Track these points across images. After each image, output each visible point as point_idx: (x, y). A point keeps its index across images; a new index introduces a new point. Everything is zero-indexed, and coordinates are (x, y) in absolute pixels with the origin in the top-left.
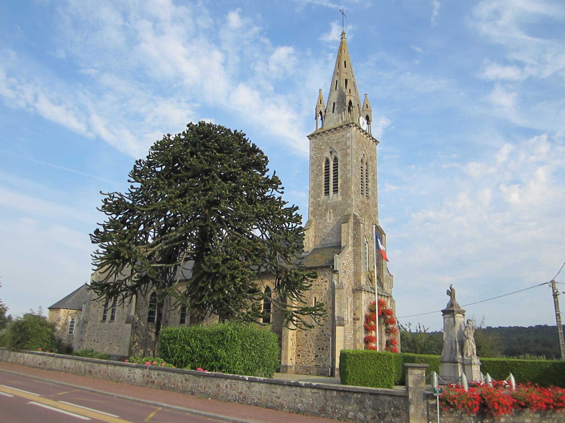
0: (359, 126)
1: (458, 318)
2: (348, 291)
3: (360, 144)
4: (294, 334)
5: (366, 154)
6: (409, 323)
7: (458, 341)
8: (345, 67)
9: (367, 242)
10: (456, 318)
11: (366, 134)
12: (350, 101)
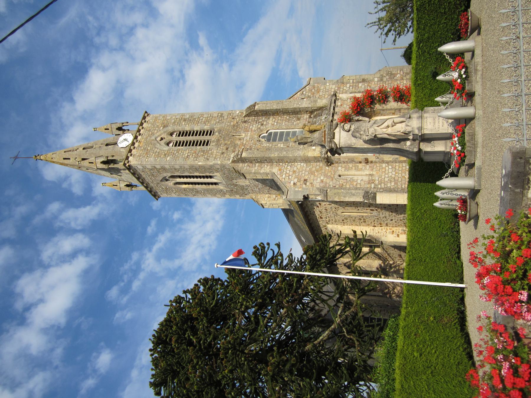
0: (130, 146)
1: (341, 141)
2: (329, 174)
3: (149, 148)
4: (391, 231)
5: (161, 135)
6: (374, 3)
7: (381, 145)
8: (69, 159)
9: (267, 133)
10: (342, 144)
11: (139, 131)
12: (101, 163)
